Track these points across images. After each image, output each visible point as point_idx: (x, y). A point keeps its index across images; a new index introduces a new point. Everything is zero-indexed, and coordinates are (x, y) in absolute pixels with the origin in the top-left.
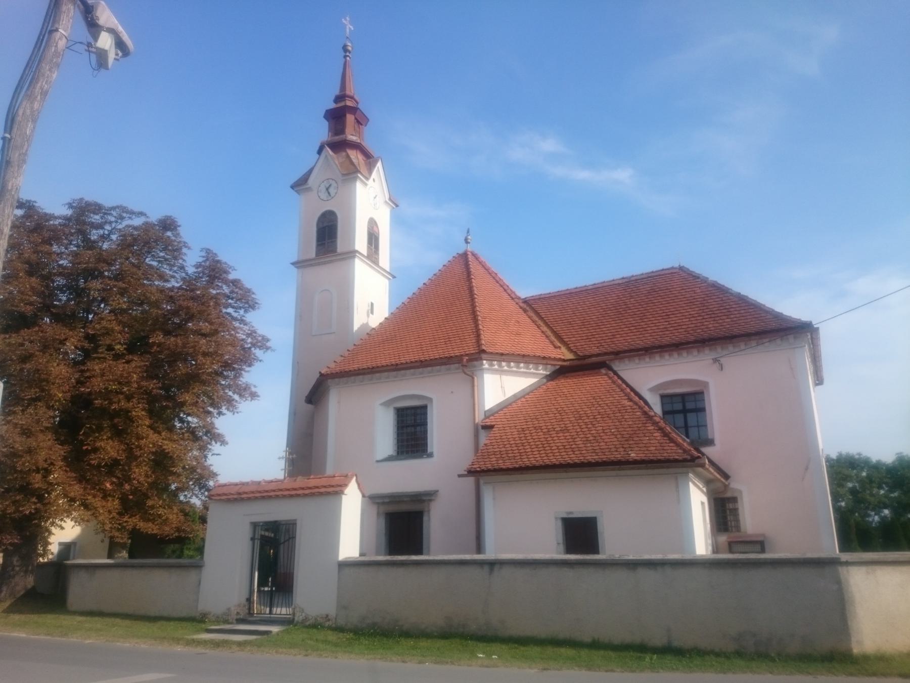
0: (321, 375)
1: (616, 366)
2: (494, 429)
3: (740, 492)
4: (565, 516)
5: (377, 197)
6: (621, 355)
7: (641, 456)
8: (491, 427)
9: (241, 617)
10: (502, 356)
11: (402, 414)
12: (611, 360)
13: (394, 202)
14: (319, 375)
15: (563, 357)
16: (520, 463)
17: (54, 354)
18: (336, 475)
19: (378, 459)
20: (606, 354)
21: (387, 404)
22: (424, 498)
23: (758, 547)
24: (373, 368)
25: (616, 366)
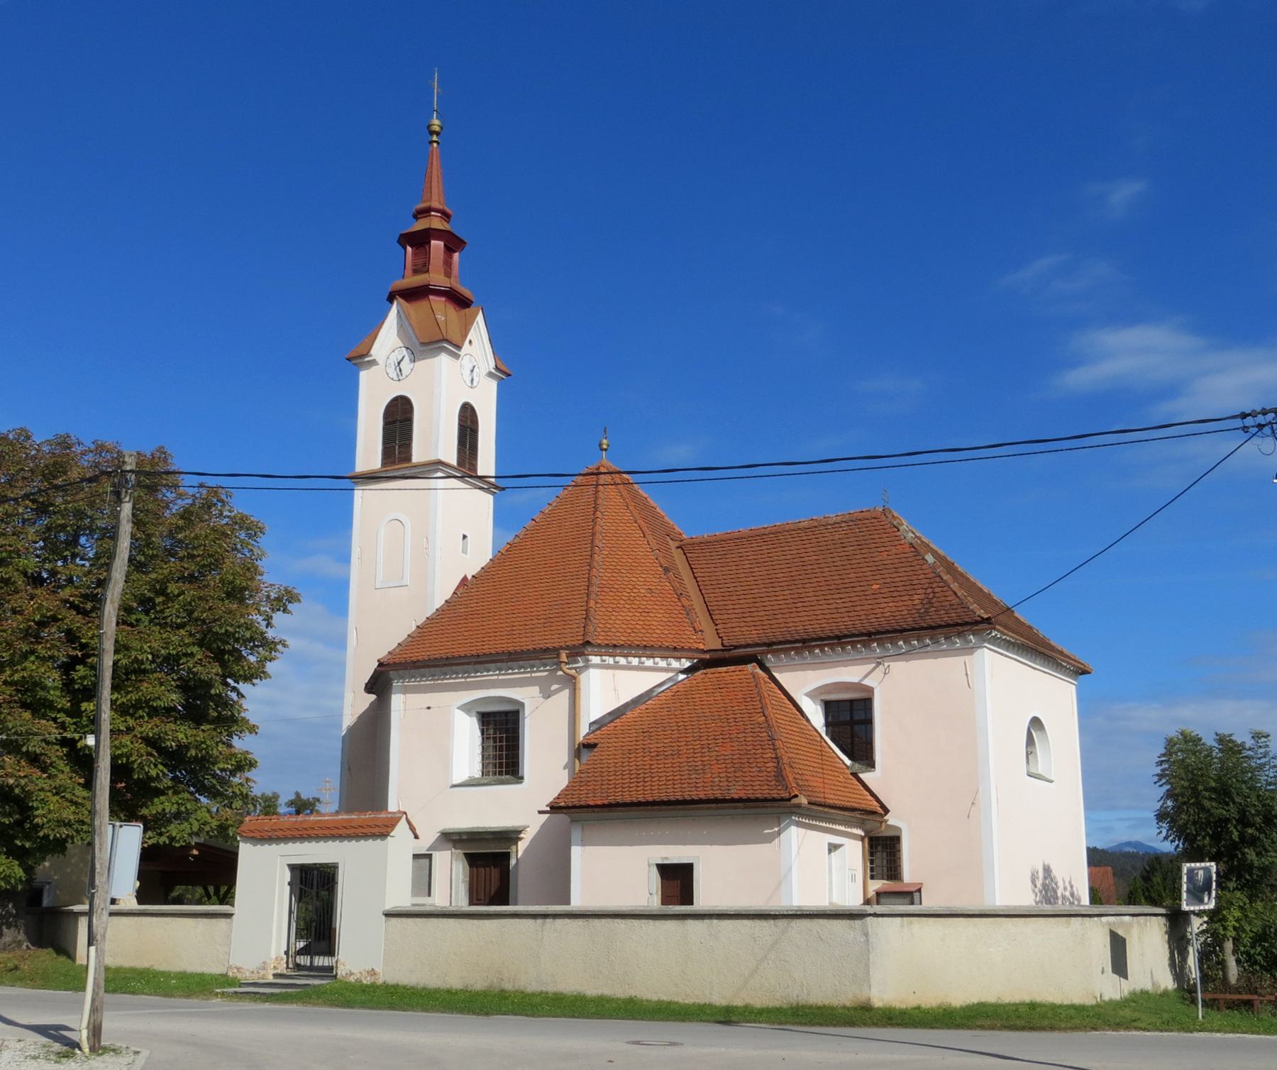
0: (381, 664)
1: (770, 660)
2: (596, 750)
3: (899, 829)
4: (660, 862)
5: (476, 369)
6: (775, 647)
7: (742, 795)
8: (595, 746)
9: (279, 972)
10: (613, 648)
11: (486, 719)
12: (763, 653)
13: (503, 374)
14: (377, 664)
15: (701, 646)
16: (612, 799)
17: (7, 507)
18: (92, 949)
19: (455, 782)
20: (757, 645)
21: (466, 708)
22: (512, 836)
23: (907, 900)
24: (447, 658)
25: (770, 660)
